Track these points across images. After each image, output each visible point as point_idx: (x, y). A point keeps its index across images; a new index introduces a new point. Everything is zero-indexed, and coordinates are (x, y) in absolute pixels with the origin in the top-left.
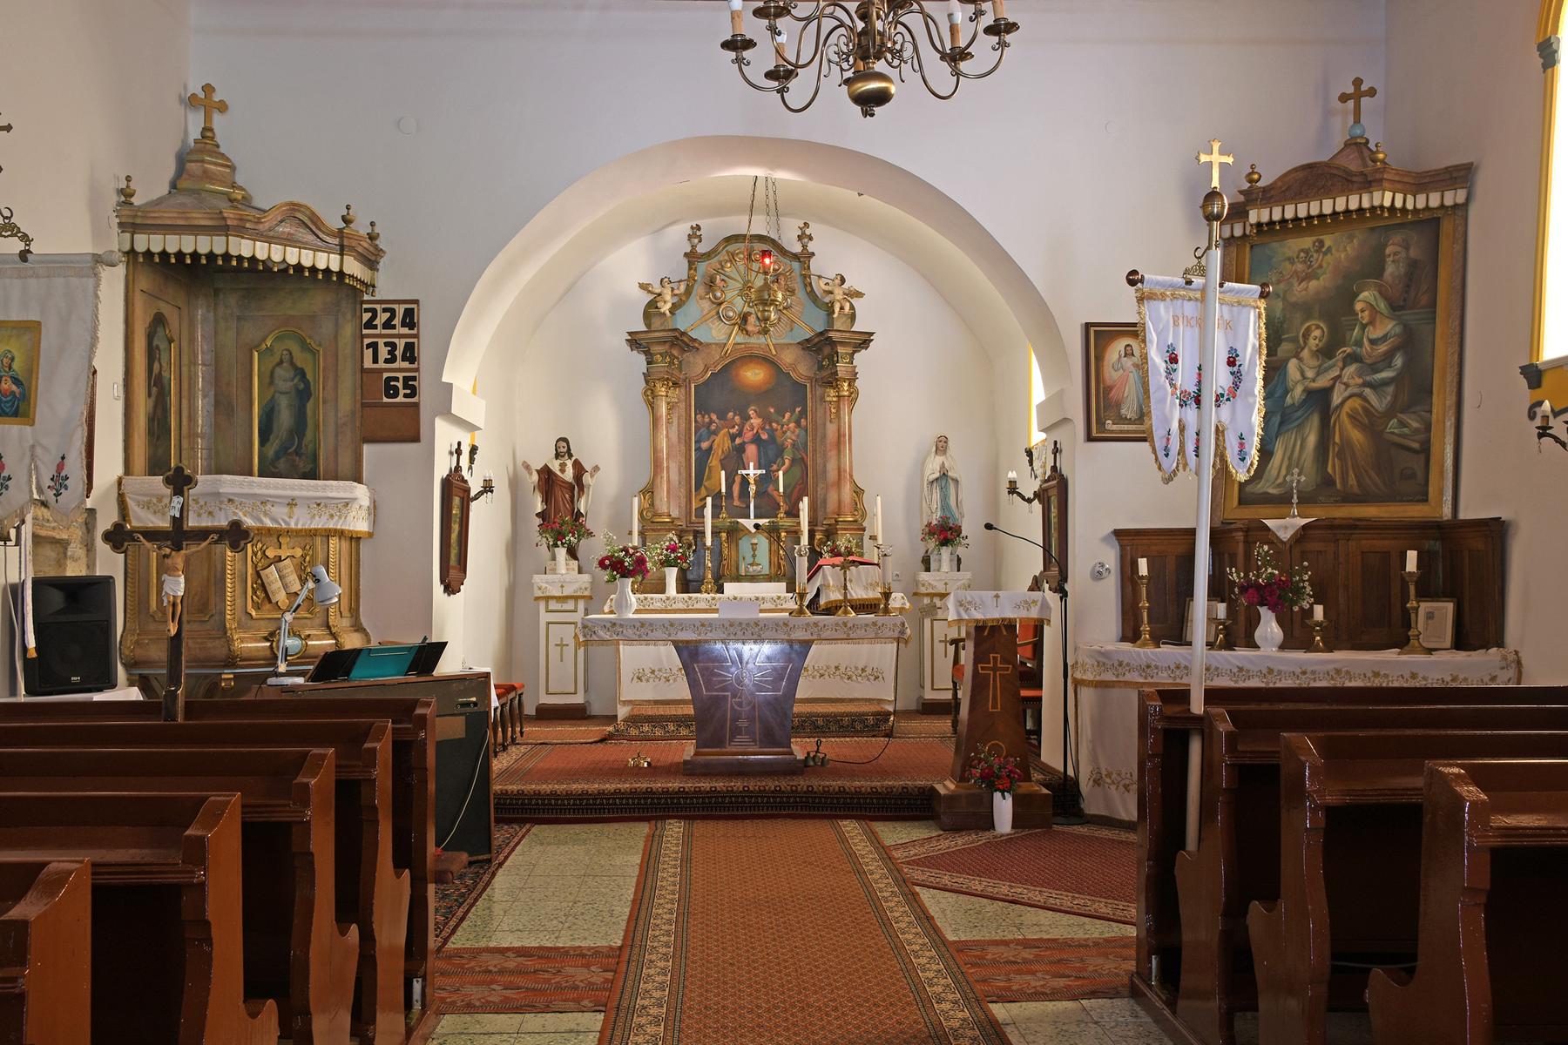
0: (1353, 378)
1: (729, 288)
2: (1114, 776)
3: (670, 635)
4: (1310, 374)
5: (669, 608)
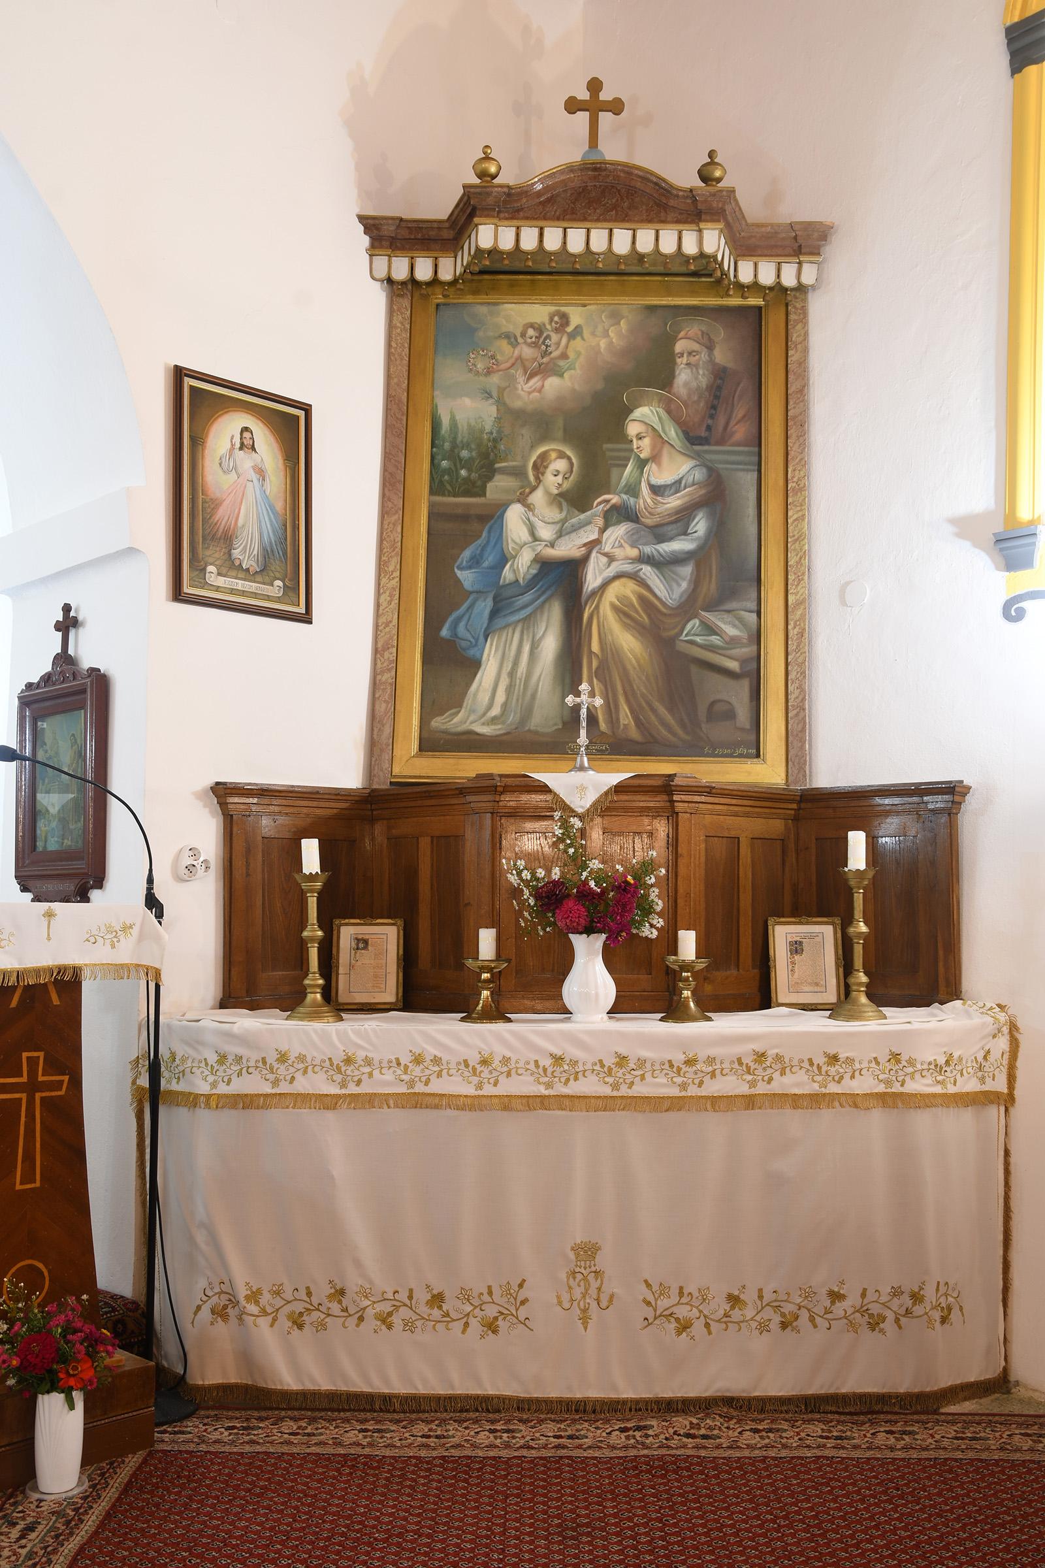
0: (621, 546)
2: (266, 1298)
4: (546, 533)
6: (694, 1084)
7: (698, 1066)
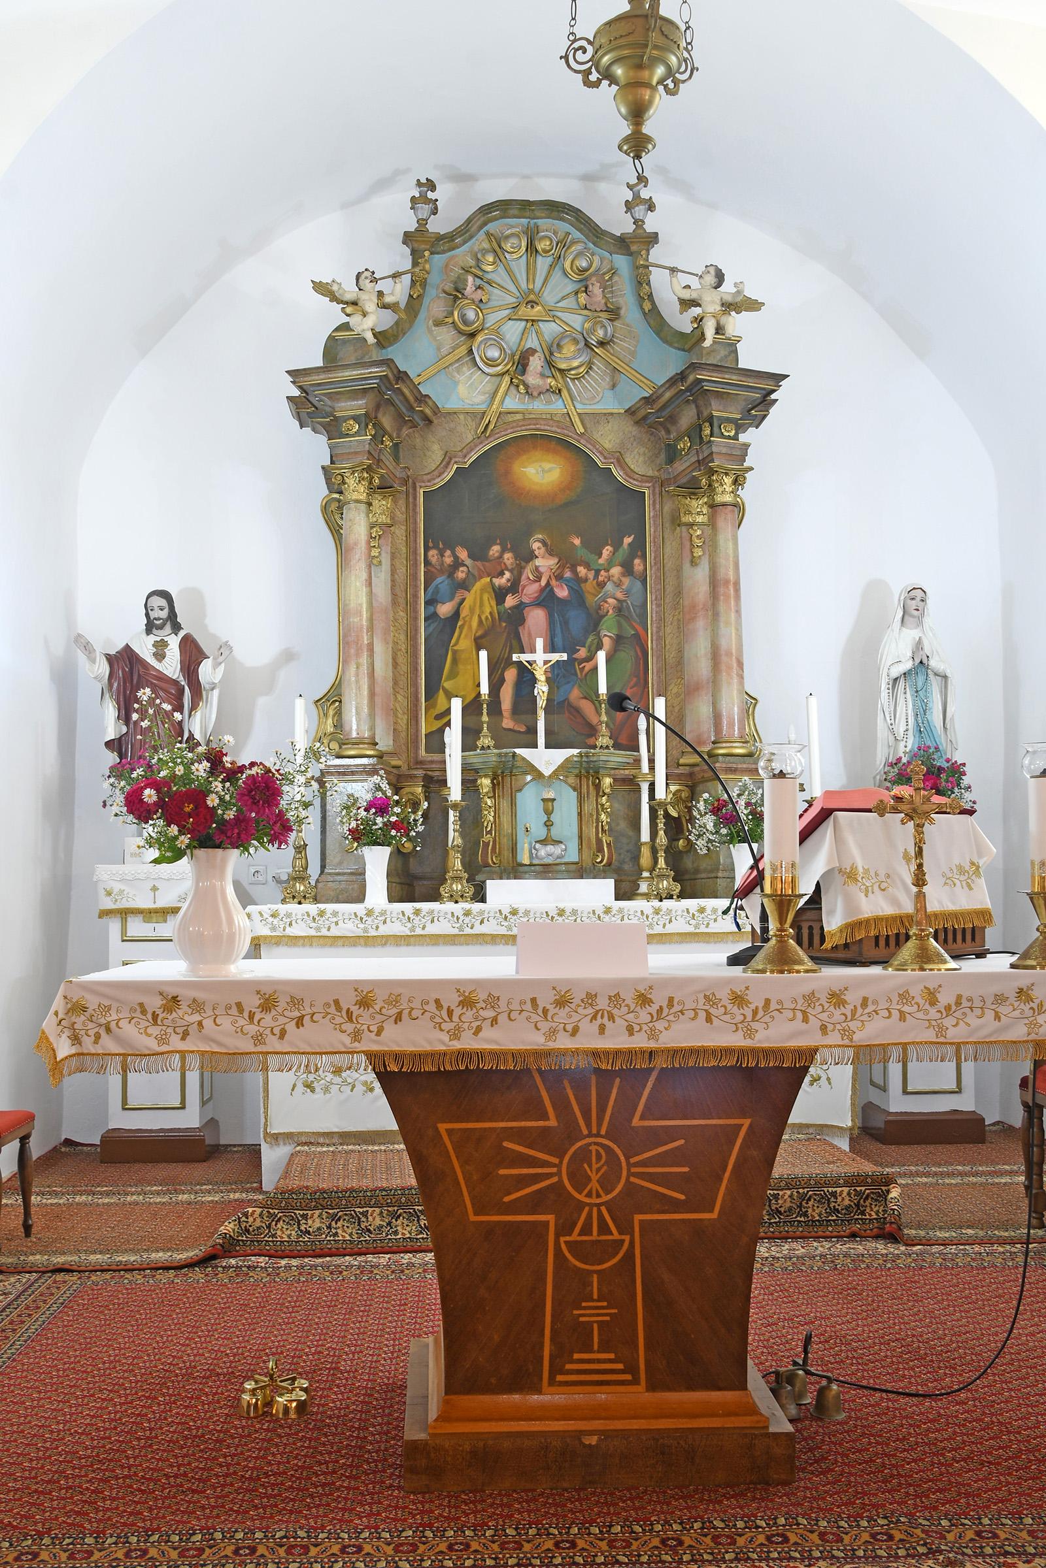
3: (356, 1036)
5: (373, 933)
6: (565, 1030)
7: (180, 1012)
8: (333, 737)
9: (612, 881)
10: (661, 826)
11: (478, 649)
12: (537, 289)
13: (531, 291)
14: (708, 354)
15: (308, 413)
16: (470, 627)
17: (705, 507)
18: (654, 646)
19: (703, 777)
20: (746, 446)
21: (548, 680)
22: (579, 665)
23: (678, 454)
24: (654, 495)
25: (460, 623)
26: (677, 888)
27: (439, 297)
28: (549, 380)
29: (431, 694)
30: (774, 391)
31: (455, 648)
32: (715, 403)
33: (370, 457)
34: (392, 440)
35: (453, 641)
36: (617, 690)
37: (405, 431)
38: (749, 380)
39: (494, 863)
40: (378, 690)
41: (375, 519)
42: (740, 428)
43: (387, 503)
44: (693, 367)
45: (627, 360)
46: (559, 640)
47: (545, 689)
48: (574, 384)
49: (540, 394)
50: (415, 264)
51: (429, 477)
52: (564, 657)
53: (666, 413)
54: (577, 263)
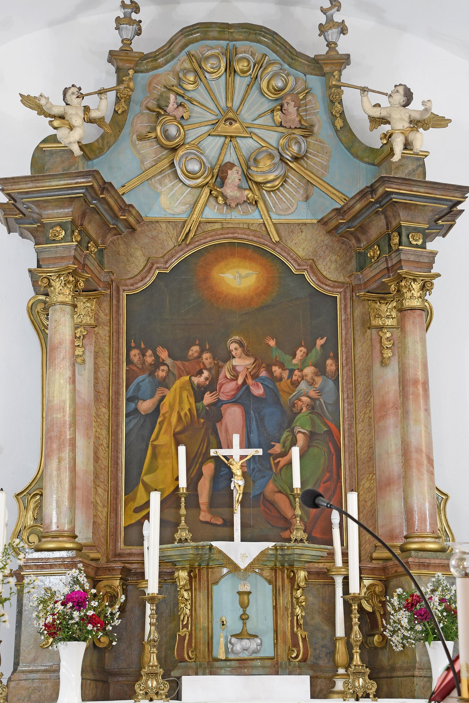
1: (191, 121)
8: (32, 530)
9: (308, 678)
10: (355, 620)
11: (177, 444)
12: (235, 108)
13: (230, 109)
14: (397, 168)
15: (16, 219)
16: (170, 423)
17: (394, 311)
18: (347, 442)
19: (396, 572)
20: (434, 254)
21: (244, 475)
22: (274, 460)
23: (368, 262)
24: (345, 299)
25: (160, 419)
26: (373, 688)
27: (142, 114)
28: (247, 192)
29: (130, 488)
30: (460, 202)
31: (155, 443)
32: (403, 214)
33: (76, 262)
34: (97, 246)
35: (153, 436)
36: (309, 487)
37: (110, 238)
38: (436, 192)
39: (190, 658)
40: (79, 483)
41: (79, 320)
42: (427, 237)
43: (91, 305)
44: (382, 180)
45: (319, 174)
46: (254, 437)
47: (241, 483)
48: (270, 197)
49: (237, 205)
50: (120, 82)
51: (132, 281)
52: (260, 452)
53: (356, 223)
54: (273, 83)
